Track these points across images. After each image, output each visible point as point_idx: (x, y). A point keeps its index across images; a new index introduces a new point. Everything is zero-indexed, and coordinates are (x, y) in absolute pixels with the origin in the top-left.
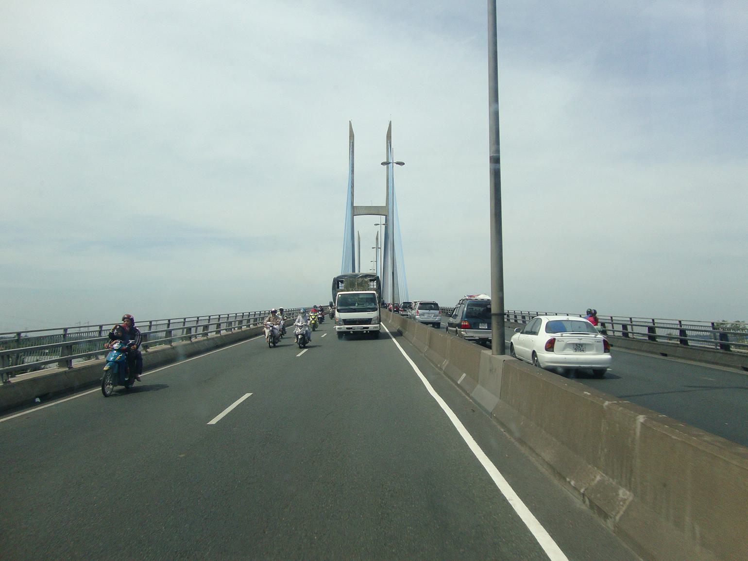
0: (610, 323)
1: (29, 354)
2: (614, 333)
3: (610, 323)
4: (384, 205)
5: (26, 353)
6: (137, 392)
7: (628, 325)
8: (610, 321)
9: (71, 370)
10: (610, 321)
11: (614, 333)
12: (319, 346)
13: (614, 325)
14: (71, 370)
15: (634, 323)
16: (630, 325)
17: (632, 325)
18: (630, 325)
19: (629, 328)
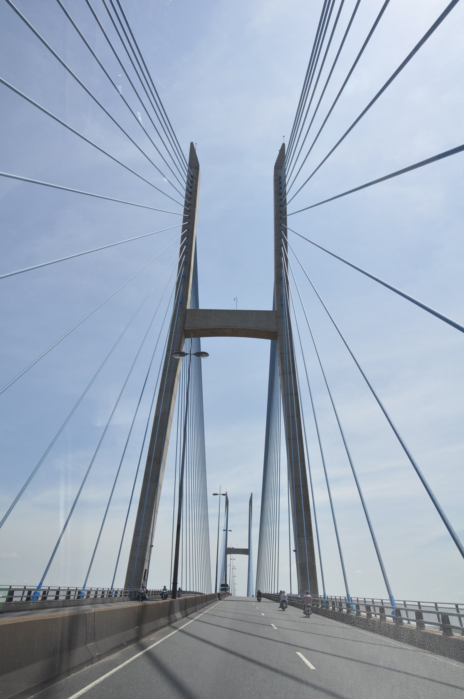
0: (434, 613)
1: (93, 593)
2: (231, 559)
3: (434, 613)
4: (247, 548)
5: (92, 597)
6: (227, 498)
7: (401, 609)
8: (434, 610)
9: (375, 618)
10: (434, 610)
11: (231, 559)
12: (303, 617)
13: (408, 611)
14: (375, 618)
15: (408, 607)
16: (403, 609)
17: (407, 610)
18: (403, 609)
19: (372, 608)
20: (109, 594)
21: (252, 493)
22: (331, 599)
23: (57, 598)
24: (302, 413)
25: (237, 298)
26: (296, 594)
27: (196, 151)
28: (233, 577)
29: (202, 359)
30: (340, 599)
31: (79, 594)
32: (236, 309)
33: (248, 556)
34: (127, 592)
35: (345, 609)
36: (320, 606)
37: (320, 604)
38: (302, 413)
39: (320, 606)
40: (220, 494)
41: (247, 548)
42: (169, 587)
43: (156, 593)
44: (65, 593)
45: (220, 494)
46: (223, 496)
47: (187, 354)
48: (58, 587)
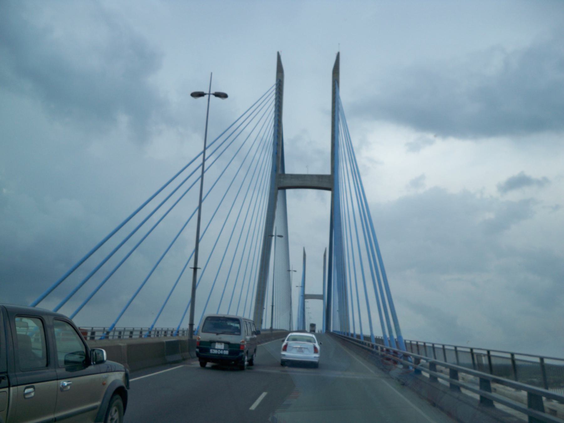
23: (141, 336)
40: (209, 94)
44: (138, 333)
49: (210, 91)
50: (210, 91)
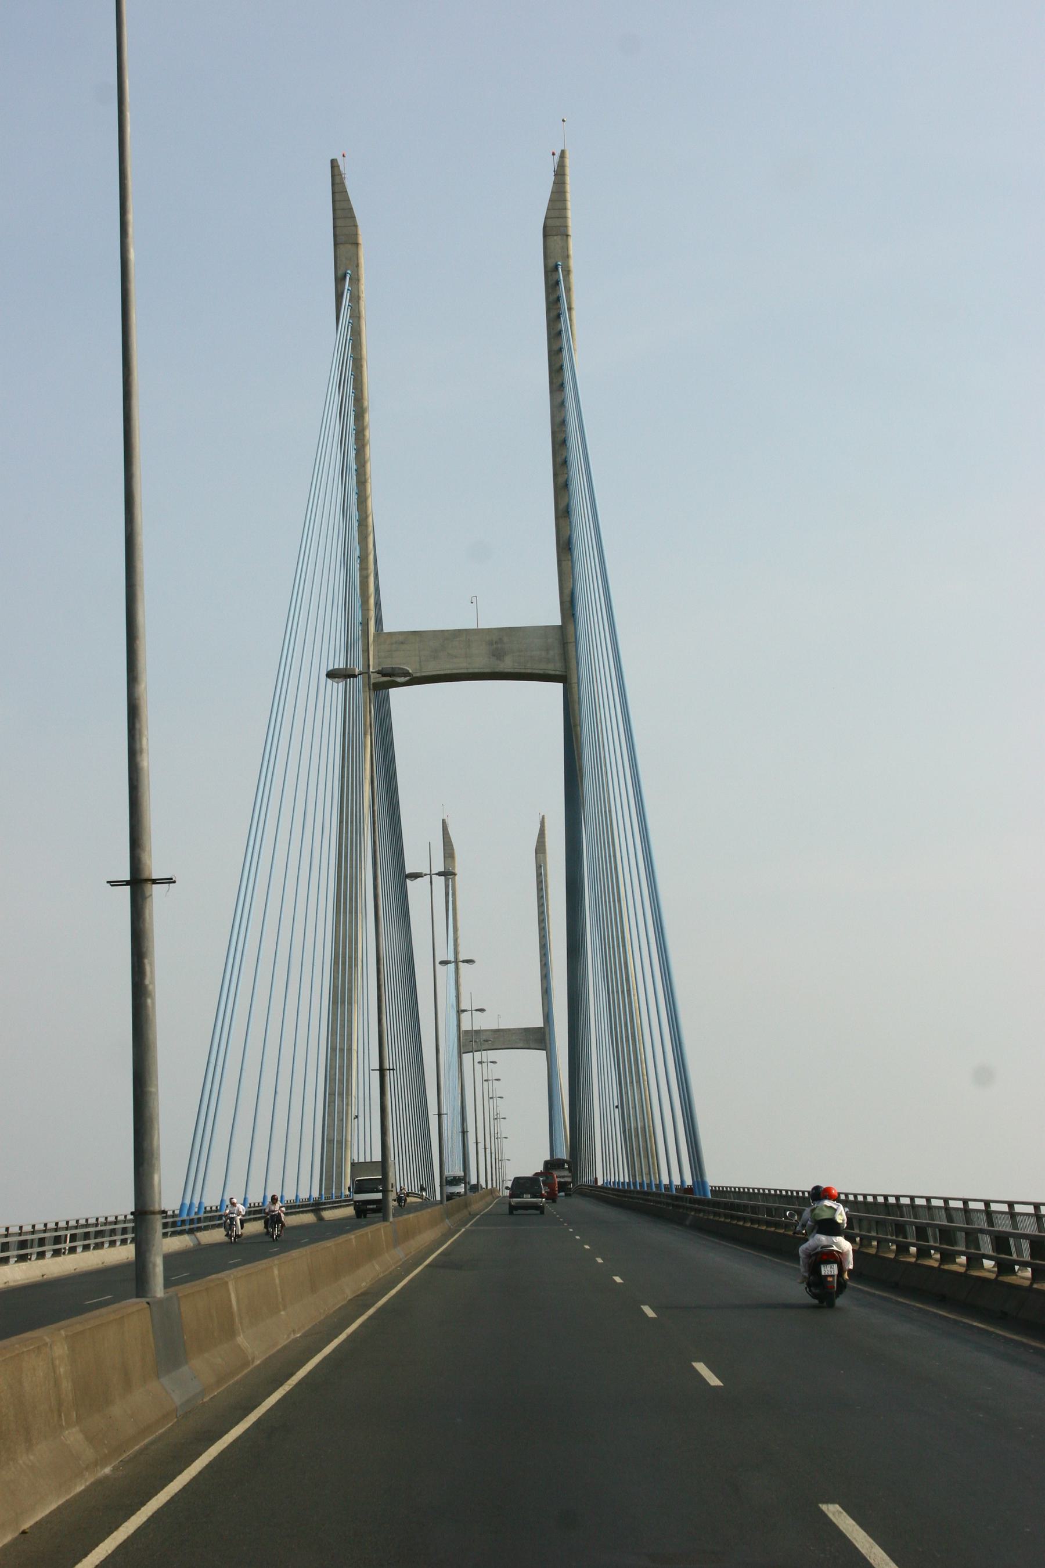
4: (540, 1023)
20: (70, 1242)
21: (543, 817)
22: (989, 1213)
24: (545, 977)
25: (476, 596)
26: (173, 1209)
27: (449, 829)
28: (496, 1140)
29: (442, 870)
30: (1012, 1215)
31: (41, 1247)
32: (476, 628)
33: (542, 1054)
34: (26, 1241)
35: (989, 1258)
36: (913, 1250)
37: (913, 1245)
38: (545, 977)
39: (913, 1250)
41: (540, 1023)
42: (124, 1205)
43: (16, 1253)
45: (471, 1011)
46: (465, 1009)
47: (426, 875)
48: (74, 1220)
49: (456, 953)
50: (456, 953)
